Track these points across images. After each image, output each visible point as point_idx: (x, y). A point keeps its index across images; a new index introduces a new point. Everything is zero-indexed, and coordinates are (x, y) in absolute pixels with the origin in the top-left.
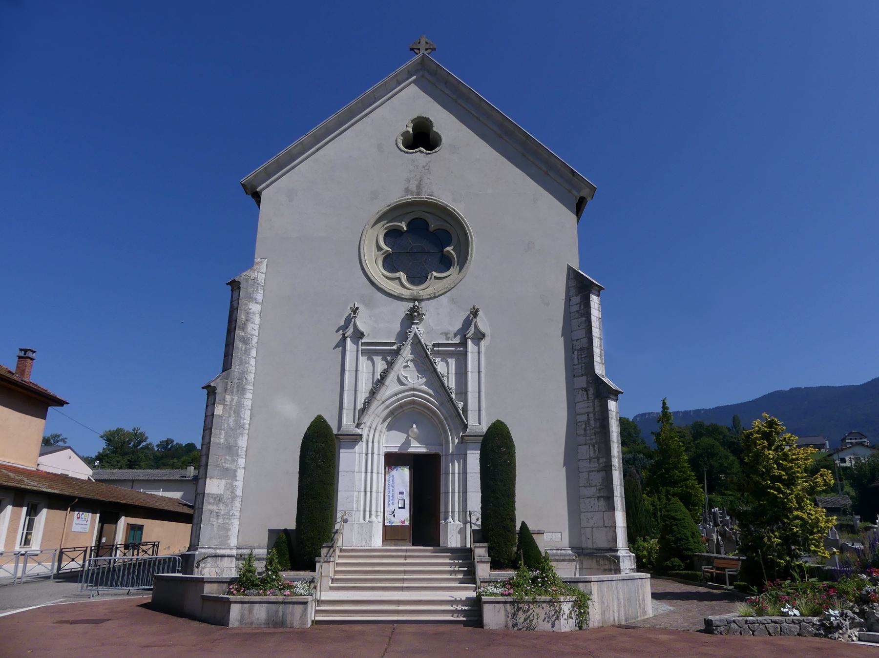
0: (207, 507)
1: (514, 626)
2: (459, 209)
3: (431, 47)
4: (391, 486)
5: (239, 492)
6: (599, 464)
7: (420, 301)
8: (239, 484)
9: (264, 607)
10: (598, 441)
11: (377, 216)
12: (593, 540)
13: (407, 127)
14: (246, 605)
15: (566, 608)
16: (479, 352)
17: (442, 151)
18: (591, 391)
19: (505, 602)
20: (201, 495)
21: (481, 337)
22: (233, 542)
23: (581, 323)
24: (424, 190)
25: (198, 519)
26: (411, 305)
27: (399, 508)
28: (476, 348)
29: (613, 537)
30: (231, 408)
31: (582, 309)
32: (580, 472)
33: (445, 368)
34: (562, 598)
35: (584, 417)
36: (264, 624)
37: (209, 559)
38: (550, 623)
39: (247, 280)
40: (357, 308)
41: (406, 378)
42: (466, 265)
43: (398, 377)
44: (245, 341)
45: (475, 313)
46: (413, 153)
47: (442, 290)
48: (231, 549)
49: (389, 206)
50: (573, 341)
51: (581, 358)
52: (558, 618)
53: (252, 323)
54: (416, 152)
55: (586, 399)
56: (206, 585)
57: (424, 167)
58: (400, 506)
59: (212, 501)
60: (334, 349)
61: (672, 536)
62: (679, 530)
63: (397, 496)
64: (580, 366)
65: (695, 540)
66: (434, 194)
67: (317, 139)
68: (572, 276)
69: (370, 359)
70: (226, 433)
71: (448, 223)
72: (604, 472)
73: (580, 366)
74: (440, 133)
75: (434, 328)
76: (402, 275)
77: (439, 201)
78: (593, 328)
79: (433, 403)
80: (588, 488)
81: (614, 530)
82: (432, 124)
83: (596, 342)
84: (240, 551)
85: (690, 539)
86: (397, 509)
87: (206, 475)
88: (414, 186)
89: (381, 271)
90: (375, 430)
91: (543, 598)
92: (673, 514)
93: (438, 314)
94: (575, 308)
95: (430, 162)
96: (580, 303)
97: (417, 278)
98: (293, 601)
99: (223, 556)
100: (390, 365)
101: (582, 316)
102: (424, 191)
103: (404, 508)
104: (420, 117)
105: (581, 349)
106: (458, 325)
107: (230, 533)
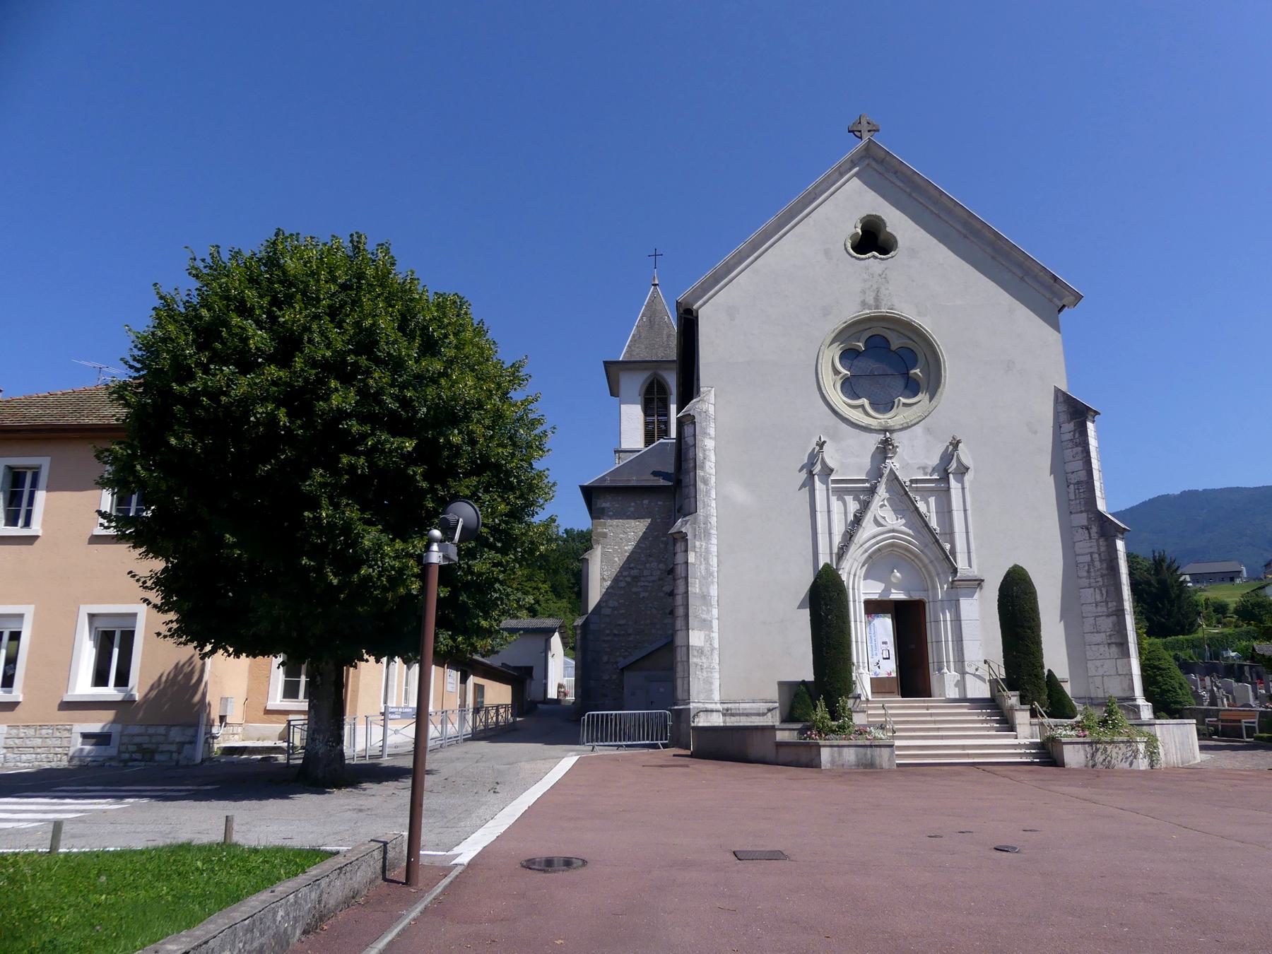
0: (693, 660)
1: (1093, 766)
2: (925, 323)
3: (874, 128)
4: (873, 636)
5: (716, 645)
6: (1108, 608)
7: (892, 431)
8: (715, 635)
9: (852, 750)
10: (1106, 584)
11: (833, 335)
12: (1104, 689)
13: (855, 227)
14: (836, 749)
15: (1142, 747)
16: (963, 489)
17: (898, 256)
18: (1094, 530)
19: (1084, 743)
20: (684, 649)
21: (964, 470)
22: (716, 697)
23: (1077, 453)
24: (883, 303)
25: (684, 672)
26: (882, 437)
27: (884, 659)
28: (960, 485)
29: (1129, 685)
30: (701, 555)
31: (1076, 437)
32: (1083, 617)
33: (928, 507)
34: (1138, 739)
35: (1088, 558)
36: (854, 765)
37: (702, 713)
38: (1128, 763)
39: (700, 413)
40: (824, 442)
41: (884, 518)
42: (940, 390)
43: (875, 517)
44: (706, 482)
45: (956, 444)
46: (866, 259)
47: (915, 418)
48: (716, 703)
49: (845, 323)
50: (1067, 473)
51: (1079, 493)
52: (1135, 757)
53: (709, 461)
54: (869, 258)
55: (1088, 538)
56: (778, 732)
57: (880, 275)
58: (885, 657)
59: (696, 653)
60: (799, 490)
61: (1158, 688)
62: (1165, 680)
63: (880, 645)
64: (1078, 501)
65: (1184, 691)
66: (894, 307)
67: (755, 246)
68: (1061, 399)
69: (841, 499)
70: (700, 582)
71: (914, 341)
72: (1115, 617)
73: (1078, 501)
74: (895, 234)
75: (910, 462)
76: (865, 401)
77: (902, 316)
78: (1092, 460)
79: (915, 545)
80: (1095, 634)
81: (1130, 678)
82: (885, 224)
83: (1096, 475)
84: (726, 706)
85: (1179, 691)
86: (881, 660)
87: (688, 626)
88: (872, 298)
89: (841, 399)
90: (855, 575)
91: (1120, 739)
92: (1156, 663)
93: (913, 446)
94: (1068, 436)
95: (886, 269)
96: (1074, 431)
97: (881, 405)
98: (881, 744)
99: (712, 711)
100: (865, 506)
101: (1077, 446)
102: (883, 304)
103: (889, 658)
104: (870, 215)
105: (1078, 483)
106: (934, 460)
107: (713, 687)
